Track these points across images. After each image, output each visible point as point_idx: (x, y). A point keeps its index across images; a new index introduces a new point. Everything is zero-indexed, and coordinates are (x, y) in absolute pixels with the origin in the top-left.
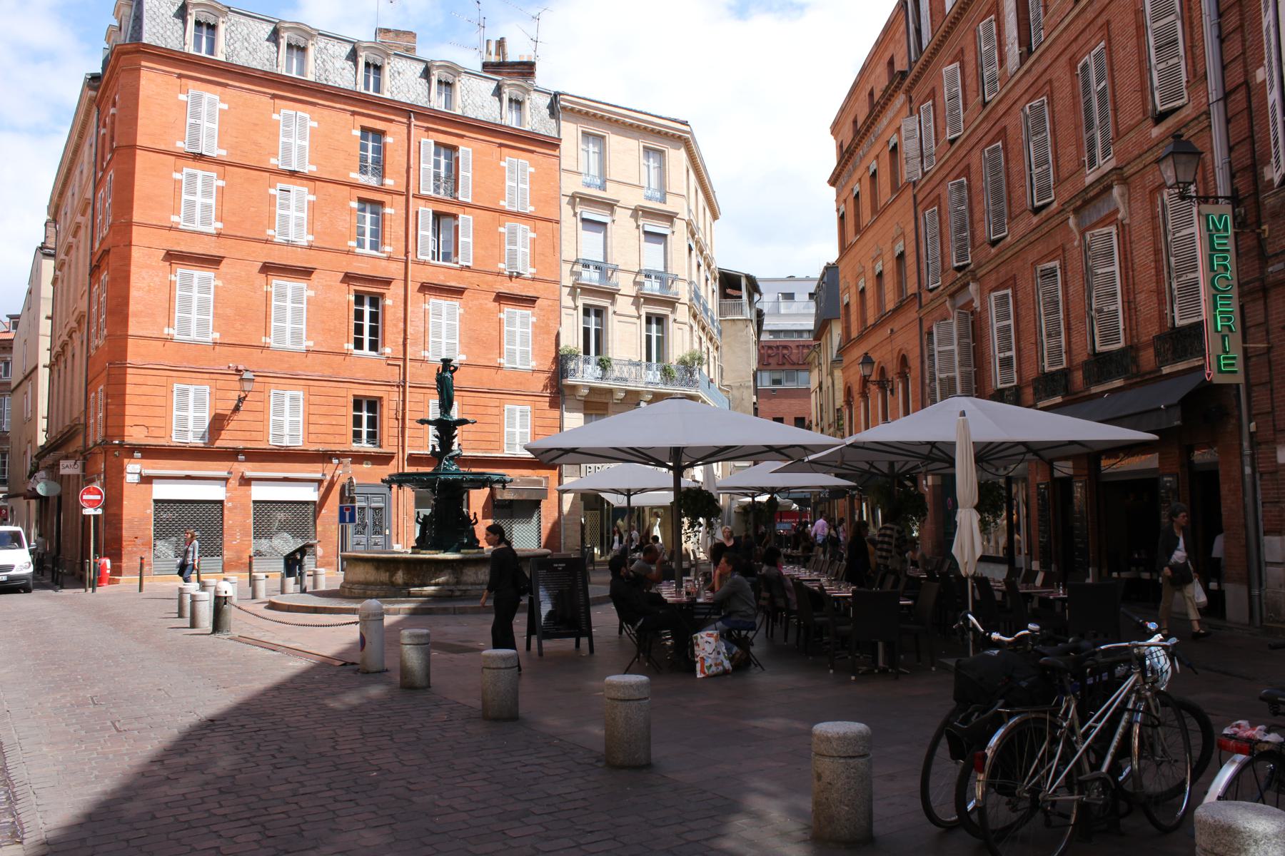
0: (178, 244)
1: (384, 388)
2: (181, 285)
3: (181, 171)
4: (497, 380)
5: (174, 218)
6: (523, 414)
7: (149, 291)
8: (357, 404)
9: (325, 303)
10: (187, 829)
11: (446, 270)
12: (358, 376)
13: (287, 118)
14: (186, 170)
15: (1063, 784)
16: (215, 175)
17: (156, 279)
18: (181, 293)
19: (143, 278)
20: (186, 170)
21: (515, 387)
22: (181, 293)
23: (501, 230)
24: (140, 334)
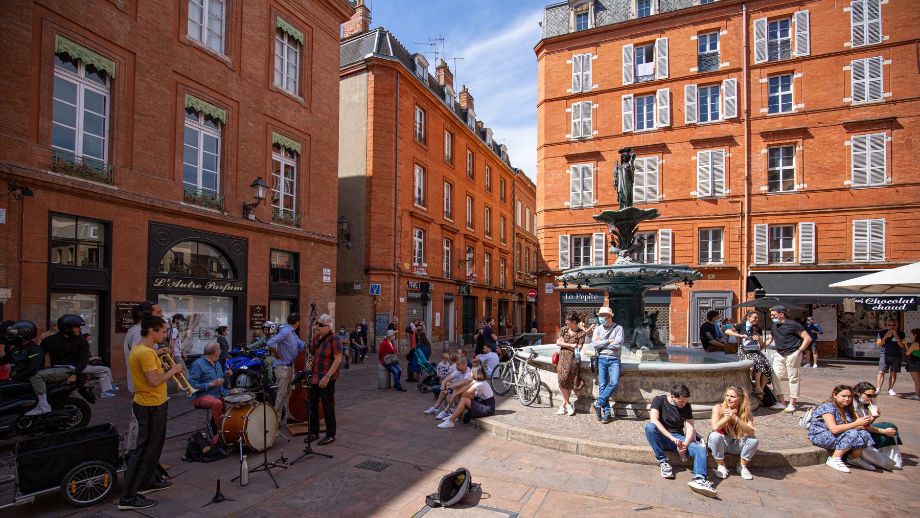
0: (571, 151)
1: (725, 220)
2: (573, 175)
3: (849, 64)
4: (843, 199)
5: (568, 136)
6: (876, 227)
7: (555, 183)
8: (704, 234)
9: (673, 166)
10: (555, 449)
11: (784, 118)
12: (703, 213)
13: (577, 60)
14: (852, 62)
15: (566, 390)
16: (881, 57)
17: (559, 175)
18: (855, 169)
19: (552, 176)
20: (573, 105)
21: (866, 203)
22: (855, 169)
23: (846, 68)
24: (551, 208)
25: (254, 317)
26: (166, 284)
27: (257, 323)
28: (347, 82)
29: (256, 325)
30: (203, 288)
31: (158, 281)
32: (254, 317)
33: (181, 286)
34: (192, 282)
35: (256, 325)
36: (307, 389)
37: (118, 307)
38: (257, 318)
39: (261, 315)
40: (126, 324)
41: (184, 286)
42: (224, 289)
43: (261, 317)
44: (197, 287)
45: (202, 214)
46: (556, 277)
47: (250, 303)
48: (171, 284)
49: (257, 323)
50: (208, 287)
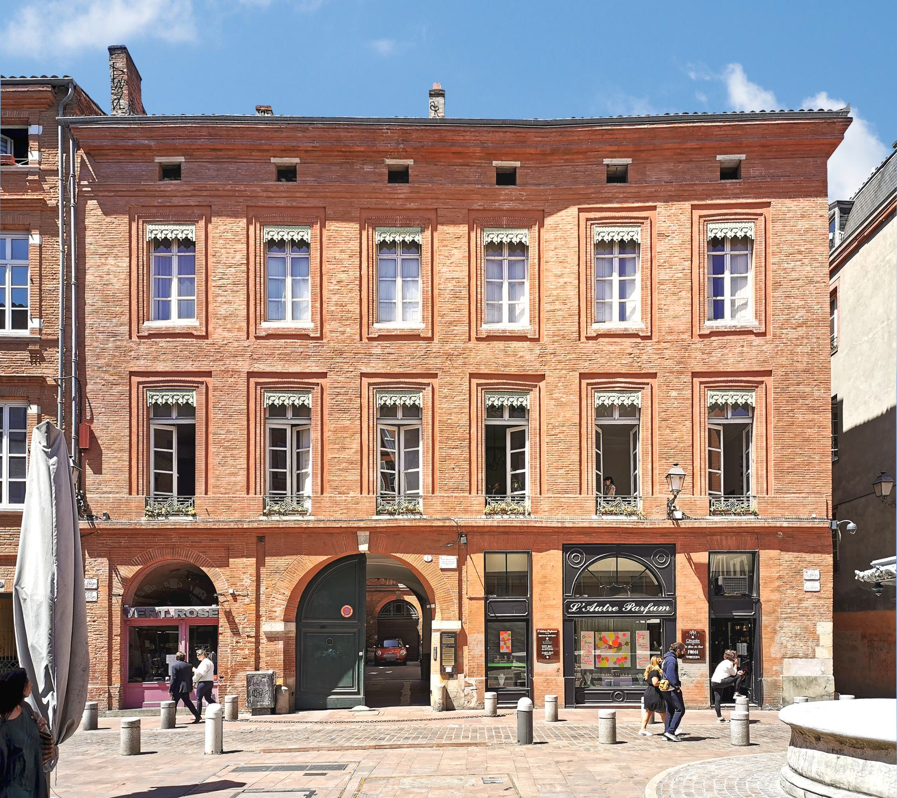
18: (393, 472)
22: (393, 472)
25: (688, 645)
26: (580, 608)
27: (692, 652)
28: (893, 226)
29: (690, 655)
30: (620, 611)
31: (573, 606)
32: (688, 645)
33: (651, 609)
34: (608, 605)
35: (690, 655)
36: (285, 690)
37: (538, 634)
38: (691, 645)
39: (698, 641)
40: (544, 651)
41: (655, 609)
42: (646, 610)
43: (697, 645)
44: (614, 609)
45: (614, 525)
46: (857, 572)
47: (680, 625)
48: (586, 609)
49: (692, 652)
50: (626, 609)
